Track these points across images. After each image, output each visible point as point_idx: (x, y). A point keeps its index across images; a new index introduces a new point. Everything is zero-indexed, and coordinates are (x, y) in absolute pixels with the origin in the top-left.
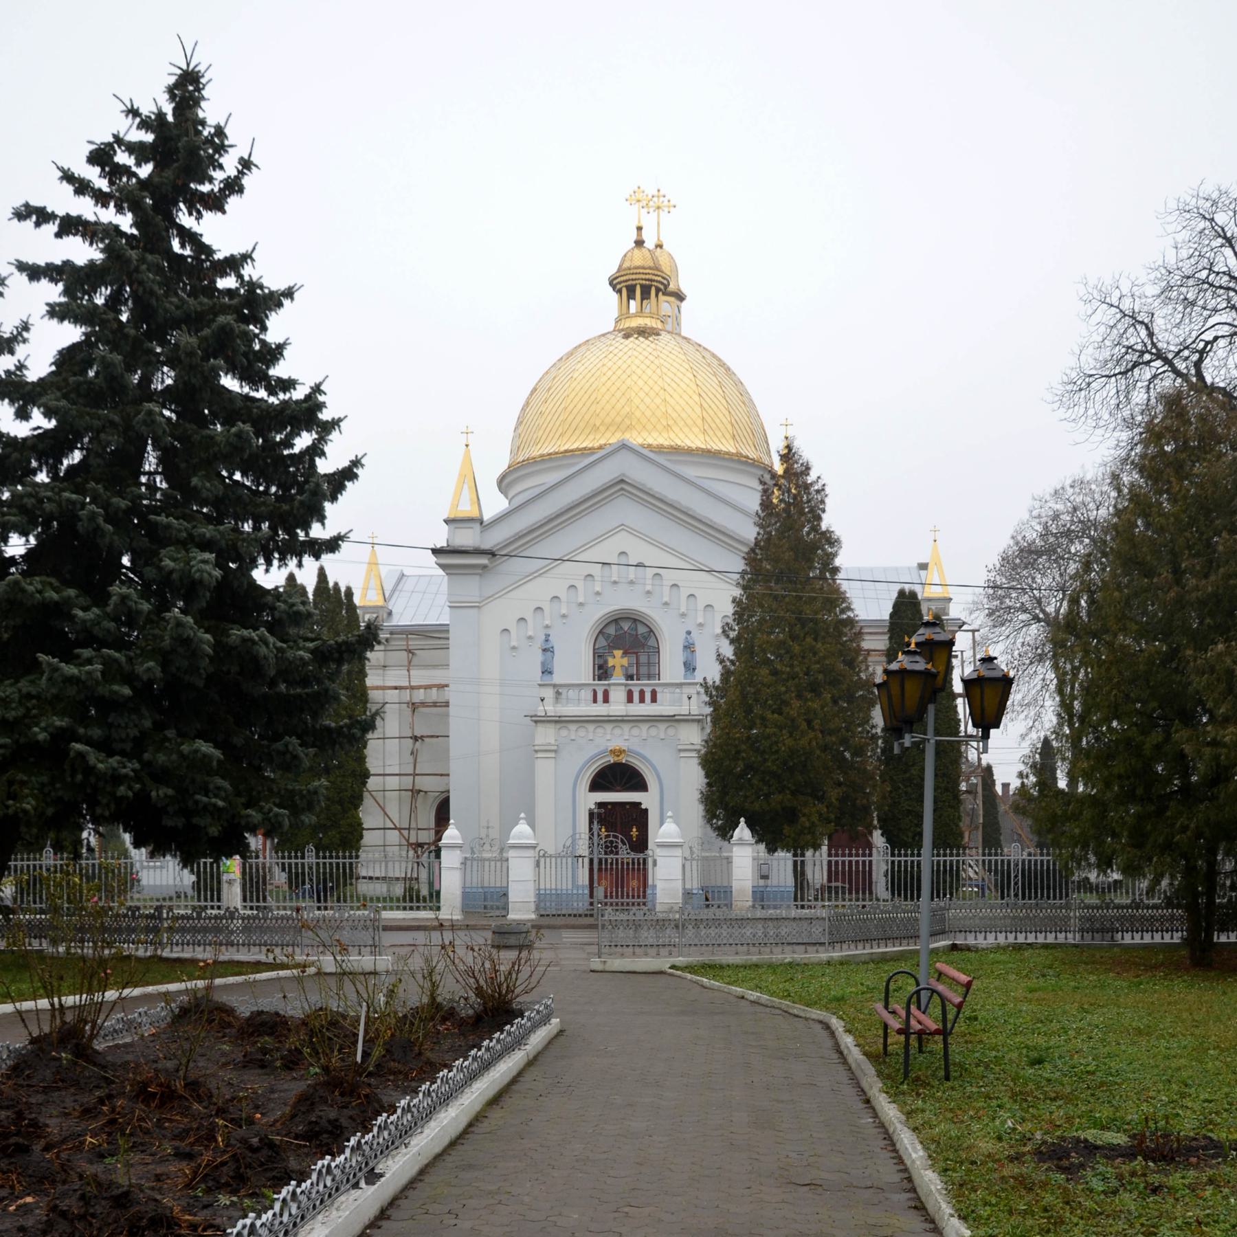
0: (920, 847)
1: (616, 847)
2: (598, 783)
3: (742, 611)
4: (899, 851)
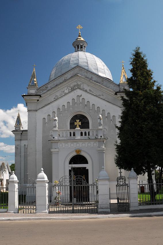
1: (81, 181)
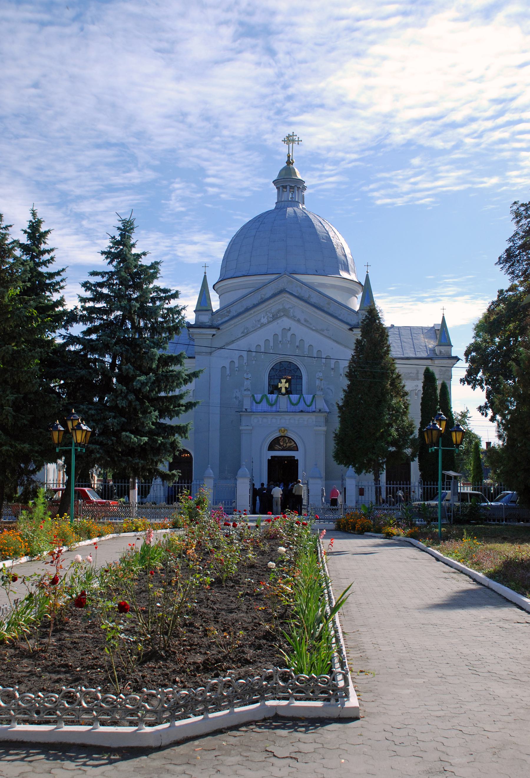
0: (437, 481)
2: (271, 448)
3: (353, 361)
4: (427, 482)
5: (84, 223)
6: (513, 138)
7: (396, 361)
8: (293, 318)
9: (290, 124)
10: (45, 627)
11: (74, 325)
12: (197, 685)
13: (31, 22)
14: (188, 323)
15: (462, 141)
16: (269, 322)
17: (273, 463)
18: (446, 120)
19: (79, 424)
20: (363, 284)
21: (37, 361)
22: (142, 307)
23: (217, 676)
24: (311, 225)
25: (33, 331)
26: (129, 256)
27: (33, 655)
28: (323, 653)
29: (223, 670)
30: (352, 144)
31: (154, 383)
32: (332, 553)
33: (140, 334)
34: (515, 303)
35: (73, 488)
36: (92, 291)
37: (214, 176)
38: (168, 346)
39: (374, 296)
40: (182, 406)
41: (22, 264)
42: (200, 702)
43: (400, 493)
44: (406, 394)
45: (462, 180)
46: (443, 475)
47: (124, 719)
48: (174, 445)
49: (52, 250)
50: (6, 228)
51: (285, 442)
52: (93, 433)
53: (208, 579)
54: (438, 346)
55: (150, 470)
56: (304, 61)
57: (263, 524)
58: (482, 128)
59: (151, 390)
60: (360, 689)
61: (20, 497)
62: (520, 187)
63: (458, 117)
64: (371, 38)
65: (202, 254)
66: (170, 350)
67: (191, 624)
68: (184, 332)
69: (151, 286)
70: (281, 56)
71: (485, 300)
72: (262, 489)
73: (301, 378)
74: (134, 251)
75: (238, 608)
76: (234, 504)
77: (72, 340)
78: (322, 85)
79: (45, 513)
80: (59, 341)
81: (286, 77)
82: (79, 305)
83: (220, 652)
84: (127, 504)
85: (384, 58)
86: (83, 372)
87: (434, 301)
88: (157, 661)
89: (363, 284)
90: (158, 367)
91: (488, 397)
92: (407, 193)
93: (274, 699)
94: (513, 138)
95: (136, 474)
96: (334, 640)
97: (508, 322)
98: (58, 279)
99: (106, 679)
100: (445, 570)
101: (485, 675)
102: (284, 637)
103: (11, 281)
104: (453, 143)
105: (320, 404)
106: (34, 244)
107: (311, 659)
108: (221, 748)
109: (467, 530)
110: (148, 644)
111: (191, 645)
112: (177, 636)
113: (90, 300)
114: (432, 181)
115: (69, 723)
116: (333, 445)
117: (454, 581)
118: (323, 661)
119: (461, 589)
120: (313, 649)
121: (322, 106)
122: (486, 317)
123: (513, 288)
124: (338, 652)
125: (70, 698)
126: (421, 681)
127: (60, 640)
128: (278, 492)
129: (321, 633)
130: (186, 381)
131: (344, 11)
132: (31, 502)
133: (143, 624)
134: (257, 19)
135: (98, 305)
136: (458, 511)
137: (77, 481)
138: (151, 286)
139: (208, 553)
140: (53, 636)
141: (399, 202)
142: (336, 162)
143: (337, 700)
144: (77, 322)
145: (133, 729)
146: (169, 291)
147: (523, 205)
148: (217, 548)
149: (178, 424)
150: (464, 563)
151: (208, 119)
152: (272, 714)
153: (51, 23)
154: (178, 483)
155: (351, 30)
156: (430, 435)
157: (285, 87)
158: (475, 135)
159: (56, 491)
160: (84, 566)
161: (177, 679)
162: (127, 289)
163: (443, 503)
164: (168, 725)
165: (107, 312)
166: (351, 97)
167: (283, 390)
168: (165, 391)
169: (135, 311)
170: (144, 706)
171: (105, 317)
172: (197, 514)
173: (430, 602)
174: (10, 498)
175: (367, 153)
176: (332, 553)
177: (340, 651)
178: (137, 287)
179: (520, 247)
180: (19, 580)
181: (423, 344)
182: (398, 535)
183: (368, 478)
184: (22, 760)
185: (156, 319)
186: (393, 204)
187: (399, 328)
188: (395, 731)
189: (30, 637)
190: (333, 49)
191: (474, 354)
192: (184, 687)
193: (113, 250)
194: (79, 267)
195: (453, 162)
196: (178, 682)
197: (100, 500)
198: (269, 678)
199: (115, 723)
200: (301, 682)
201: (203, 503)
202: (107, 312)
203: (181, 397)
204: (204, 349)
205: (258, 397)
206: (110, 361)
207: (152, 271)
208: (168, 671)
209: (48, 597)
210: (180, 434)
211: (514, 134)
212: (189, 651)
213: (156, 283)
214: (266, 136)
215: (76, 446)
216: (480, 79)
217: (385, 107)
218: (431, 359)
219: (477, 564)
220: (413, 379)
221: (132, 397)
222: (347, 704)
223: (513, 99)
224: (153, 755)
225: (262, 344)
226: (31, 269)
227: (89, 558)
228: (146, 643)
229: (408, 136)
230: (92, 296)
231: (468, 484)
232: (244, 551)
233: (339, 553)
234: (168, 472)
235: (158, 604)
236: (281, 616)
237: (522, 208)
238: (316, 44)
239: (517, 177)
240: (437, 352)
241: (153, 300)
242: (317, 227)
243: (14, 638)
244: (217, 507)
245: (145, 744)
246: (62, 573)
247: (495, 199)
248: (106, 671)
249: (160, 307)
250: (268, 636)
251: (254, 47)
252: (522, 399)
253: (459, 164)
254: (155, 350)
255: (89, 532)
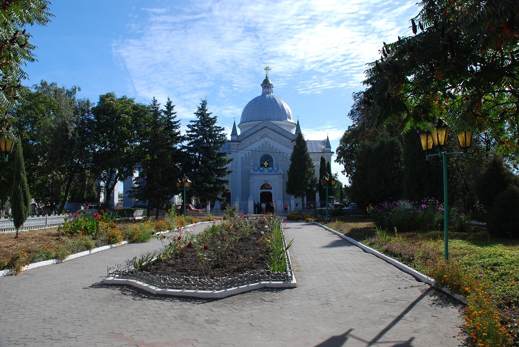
2: (261, 188)
3: (293, 154)
5: (187, 103)
6: (350, 69)
7: (310, 154)
8: (269, 137)
9: (266, 63)
10: (176, 256)
11: (184, 141)
12: (235, 276)
13: (167, 30)
14: (228, 140)
15: (331, 70)
16: (260, 139)
17: (262, 194)
18: (325, 62)
19: (187, 180)
20: (296, 124)
21: (170, 156)
22: (210, 134)
23: (242, 273)
24: (276, 102)
25: (169, 144)
26: (205, 114)
27: (172, 266)
28: (283, 264)
29: (244, 271)
30: (290, 71)
31: (215, 163)
32: (286, 228)
33: (210, 145)
34: (355, 131)
35: (185, 205)
36: (191, 128)
37: (236, 84)
38: (220, 149)
39: (301, 129)
40: (226, 172)
41: (164, 118)
42: (236, 282)
43: (312, 205)
44: (314, 166)
45: (332, 84)
46: (328, 197)
47: (207, 288)
48: (223, 188)
49: (176, 113)
50: (158, 105)
51: (267, 186)
52: (192, 183)
53: (238, 238)
54: (326, 147)
55: (214, 198)
56: (270, 40)
57: (259, 218)
58: (338, 65)
59: (214, 166)
60: (297, 277)
61: (165, 208)
62: (354, 87)
63: (329, 61)
64: (295, 32)
65: (232, 114)
66: (221, 150)
67: (232, 255)
68: (227, 144)
69: (214, 126)
70: (261, 38)
71: (342, 130)
72: (258, 205)
73: (273, 161)
74: (207, 112)
75: (250, 249)
76: (247, 210)
77: (184, 147)
78: (277, 49)
79: (175, 214)
80: (179, 148)
81: (263, 46)
82: (186, 134)
83: (243, 265)
84: (206, 211)
85: (301, 39)
86: (188, 160)
87: (323, 131)
88: (219, 268)
89: (296, 124)
90: (217, 157)
91: (345, 167)
92: (311, 89)
93: (264, 281)
94: (350, 69)
95: (209, 199)
96: (287, 260)
97: (352, 138)
98: (178, 124)
99: (200, 274)
100: (329, 233)
101: (344, 270)
102: (267, 259)
103: (160, 125)
104: (328, 71)
105: (280, 171)
106: (169, 110)
107: (278, 266)
108: (244, 298)
109: (337, 218)
110: (216, 262)
111: (232, 262)
112: (226, 259)
113: (190, 132)
114: (320, 85)
115: (187, 289)
116: (285, 187)
117: (332, 237)
118: (283, 267)
119: (335, 240)
120: (279, 263)
121: (277, 57)
122: (344, 136)
123: (353, 125)
124: (288, 264)
125: (186, 280)
126: (320, 273)
127: (182, 260)
128: (264, 205)
129: (282, 257)
130: (228, 163)
131: (284, 22)
132: (169, 210)
133: (213, 254)
134: (252, 25)
135: (193, 134)
136: (334, 211)
137: (187, 202)
138: (214, 126)
139: (238, 229)
140: (179, 259)
141: (308, 92)
142: (283, 78)
143: (288, 281)
144: (185, 140)
145: (211, 292)
146: (221, 127)
147: (356, 93)
148: (241, 227)
149: (225, 179)
150: (336, 231)
151: (234, 62)
152: (263, 287)
153: (174, 30)
154: (225, 202)
155: (288, 29)
156: (323, 182)
157: (263, 50)
158: (336, 68)
159: (178, 206)
160: (190, 233)
161: (227, 274)
162: (204, 127)
163: (328, 208)
164: (224, 290)
165: (197, 136)
166: (288, 53)
167: (266, 166)
168: (220, 167)
169: (208, 136)
170: (215, 284)
171: (196, 138)
172: (233, 214)
173: (323, 245)
174: (161, 209)
175: (295, 74)
176: (286, 228)
177: (289, 264)
178: (208, 126)
179: (356, 110)
180: (166, 238)
181: (320, 147)
182: (311, 221)
183: (299, 200)
184: (171, 301)
185: (216, 139)
186: (306, 93)
187: (310, 141)
188: (310, 291)
189: (171, 259)
190: (281, 36)
191: (339, 151)
192: (230, 277)
193: (199, 112)
194: (185, 120)
195: (328, 78)
196: (227, 276)
197: (195, 209)
198: (262, 274)
199: (204, 289)
200: (274, 275)
201: (235, 210)
202: (197, 136)
203: (226, 169)
204: (235, 150)
205: (256, 169)
206: (198, 155)
207: (214, 120)
208: (223, 272)
209: (177, 245)
210: (226, 184)
211: (350, 67)
212: (231, 264)
213: (216, 125)
214: (256, 68)
215: (186, 188)
216: (337, 47)
217: (301, 57)
218: (323, 153)
219: (341, 231)
220: (316, 161)
221: (207, 169)
222: (292, 282)
223: (349, 55)
224: (219, 301)
225: (257, 148)
226: (168, 120)
227: (192, 230)
228: (215, 261)
229: (311, 68)
230: (191, 130)
231: (337, 202)
232: (252, 227)
233: (288, 228)
234: (221, 198)
235: (219, 247)
236: (266, 252)
237: (356, 95)
238: (274, 34)
239: (352, 83)
240: (325, 150)
241: (215, 131)
242: (278, 102)
243: (165, 259)
244: (241, 211)
245: (216, 297)
246: (182, 235)
247: (345, 91)
248: (200, 271)
249: (217, 134)
250: (261, 259)
251: (250, 35)
252: (358, 168)
253: (330, 78)
254: (216, 151)
255: (192, 221)
